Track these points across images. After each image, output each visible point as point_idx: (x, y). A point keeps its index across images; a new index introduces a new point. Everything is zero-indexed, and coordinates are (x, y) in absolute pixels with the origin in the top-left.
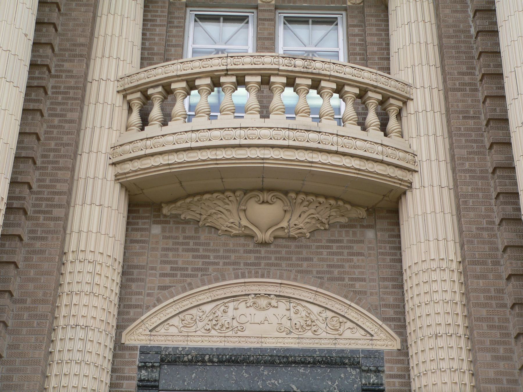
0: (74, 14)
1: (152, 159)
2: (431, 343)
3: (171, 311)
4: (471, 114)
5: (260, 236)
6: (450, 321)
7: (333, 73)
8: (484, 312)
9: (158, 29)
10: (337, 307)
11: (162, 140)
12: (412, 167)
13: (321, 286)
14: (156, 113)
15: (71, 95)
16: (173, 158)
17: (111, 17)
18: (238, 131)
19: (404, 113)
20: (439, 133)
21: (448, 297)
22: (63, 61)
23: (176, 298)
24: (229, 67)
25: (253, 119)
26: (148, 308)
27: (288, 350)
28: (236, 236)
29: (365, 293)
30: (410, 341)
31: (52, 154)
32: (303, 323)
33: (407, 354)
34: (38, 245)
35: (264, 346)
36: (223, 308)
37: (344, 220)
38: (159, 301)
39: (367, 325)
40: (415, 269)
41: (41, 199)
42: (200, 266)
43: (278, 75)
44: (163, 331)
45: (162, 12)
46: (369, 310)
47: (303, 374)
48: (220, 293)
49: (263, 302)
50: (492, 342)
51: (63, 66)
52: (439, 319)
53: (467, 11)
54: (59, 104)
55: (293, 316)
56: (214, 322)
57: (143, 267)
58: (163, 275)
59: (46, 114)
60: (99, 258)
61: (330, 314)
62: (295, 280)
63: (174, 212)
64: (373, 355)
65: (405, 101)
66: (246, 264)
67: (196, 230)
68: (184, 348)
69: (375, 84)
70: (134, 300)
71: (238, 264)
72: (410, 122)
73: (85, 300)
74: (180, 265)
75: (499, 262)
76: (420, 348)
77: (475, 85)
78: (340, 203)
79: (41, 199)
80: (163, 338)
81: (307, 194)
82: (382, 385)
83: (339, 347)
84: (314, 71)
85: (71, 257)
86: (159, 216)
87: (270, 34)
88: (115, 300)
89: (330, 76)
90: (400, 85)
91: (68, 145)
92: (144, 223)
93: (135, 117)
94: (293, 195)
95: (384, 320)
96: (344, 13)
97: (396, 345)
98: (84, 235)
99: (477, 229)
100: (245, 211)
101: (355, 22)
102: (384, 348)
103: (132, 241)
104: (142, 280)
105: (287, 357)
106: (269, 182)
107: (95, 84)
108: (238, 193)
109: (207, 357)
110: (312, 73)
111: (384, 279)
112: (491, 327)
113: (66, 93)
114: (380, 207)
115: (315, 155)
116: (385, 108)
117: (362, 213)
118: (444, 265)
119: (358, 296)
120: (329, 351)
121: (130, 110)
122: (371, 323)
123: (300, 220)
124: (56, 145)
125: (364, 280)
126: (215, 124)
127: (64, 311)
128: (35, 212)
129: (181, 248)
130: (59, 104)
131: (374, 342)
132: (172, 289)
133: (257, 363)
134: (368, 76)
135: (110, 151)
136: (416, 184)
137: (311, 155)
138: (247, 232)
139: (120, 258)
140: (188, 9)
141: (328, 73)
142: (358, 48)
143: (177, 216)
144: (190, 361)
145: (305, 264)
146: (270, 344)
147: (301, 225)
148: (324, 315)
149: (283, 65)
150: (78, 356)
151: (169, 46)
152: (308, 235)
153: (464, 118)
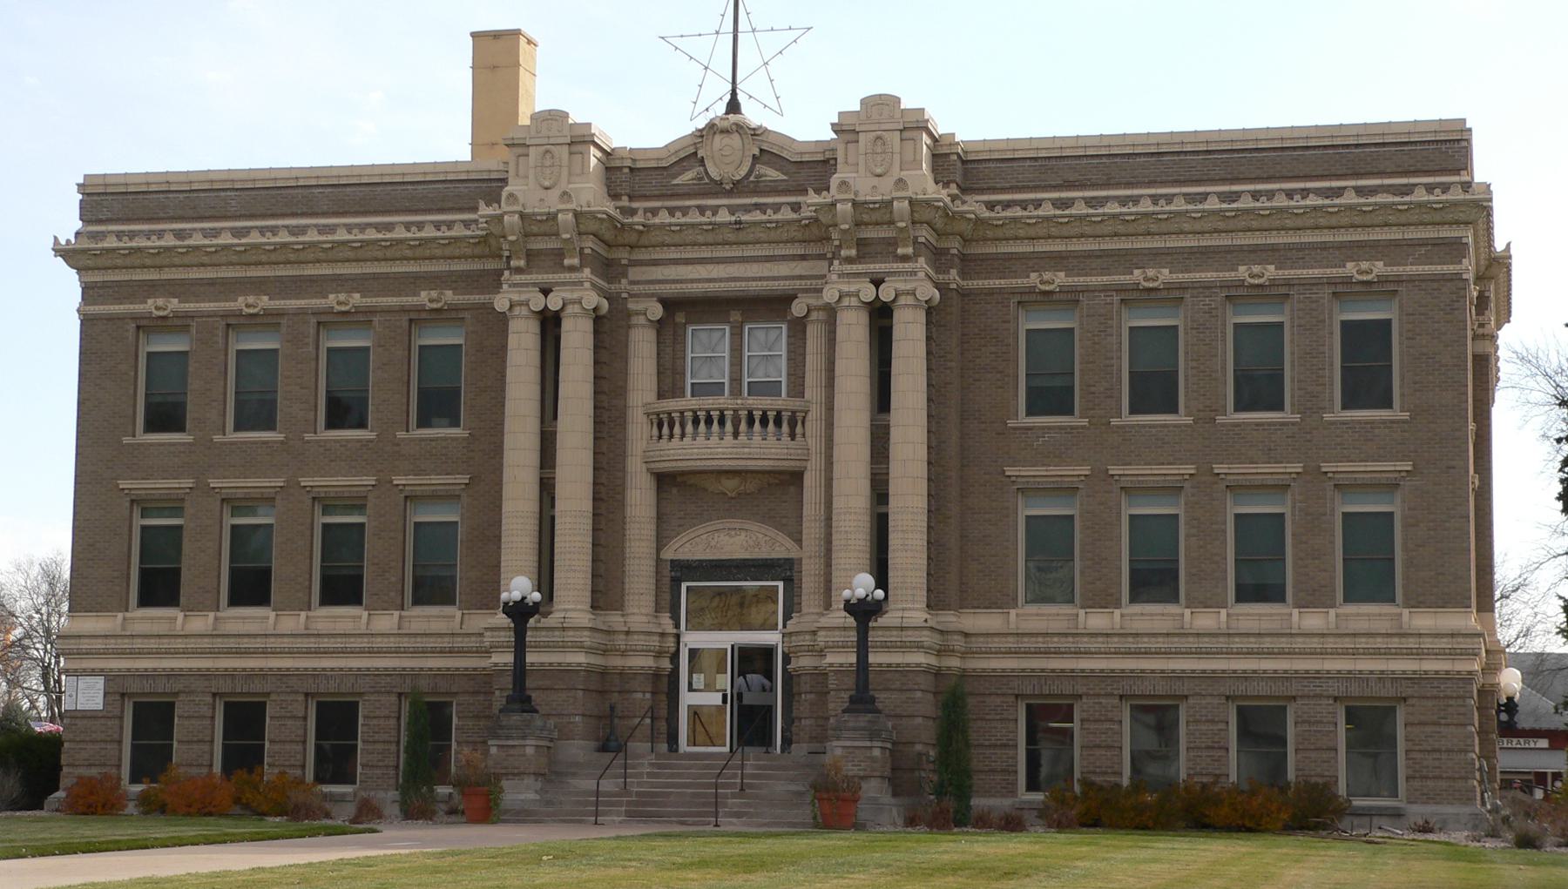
14: (665, 430)
93: (655, 431)
114: (795, 478)
119: (780, 527)
122: (789, 543)
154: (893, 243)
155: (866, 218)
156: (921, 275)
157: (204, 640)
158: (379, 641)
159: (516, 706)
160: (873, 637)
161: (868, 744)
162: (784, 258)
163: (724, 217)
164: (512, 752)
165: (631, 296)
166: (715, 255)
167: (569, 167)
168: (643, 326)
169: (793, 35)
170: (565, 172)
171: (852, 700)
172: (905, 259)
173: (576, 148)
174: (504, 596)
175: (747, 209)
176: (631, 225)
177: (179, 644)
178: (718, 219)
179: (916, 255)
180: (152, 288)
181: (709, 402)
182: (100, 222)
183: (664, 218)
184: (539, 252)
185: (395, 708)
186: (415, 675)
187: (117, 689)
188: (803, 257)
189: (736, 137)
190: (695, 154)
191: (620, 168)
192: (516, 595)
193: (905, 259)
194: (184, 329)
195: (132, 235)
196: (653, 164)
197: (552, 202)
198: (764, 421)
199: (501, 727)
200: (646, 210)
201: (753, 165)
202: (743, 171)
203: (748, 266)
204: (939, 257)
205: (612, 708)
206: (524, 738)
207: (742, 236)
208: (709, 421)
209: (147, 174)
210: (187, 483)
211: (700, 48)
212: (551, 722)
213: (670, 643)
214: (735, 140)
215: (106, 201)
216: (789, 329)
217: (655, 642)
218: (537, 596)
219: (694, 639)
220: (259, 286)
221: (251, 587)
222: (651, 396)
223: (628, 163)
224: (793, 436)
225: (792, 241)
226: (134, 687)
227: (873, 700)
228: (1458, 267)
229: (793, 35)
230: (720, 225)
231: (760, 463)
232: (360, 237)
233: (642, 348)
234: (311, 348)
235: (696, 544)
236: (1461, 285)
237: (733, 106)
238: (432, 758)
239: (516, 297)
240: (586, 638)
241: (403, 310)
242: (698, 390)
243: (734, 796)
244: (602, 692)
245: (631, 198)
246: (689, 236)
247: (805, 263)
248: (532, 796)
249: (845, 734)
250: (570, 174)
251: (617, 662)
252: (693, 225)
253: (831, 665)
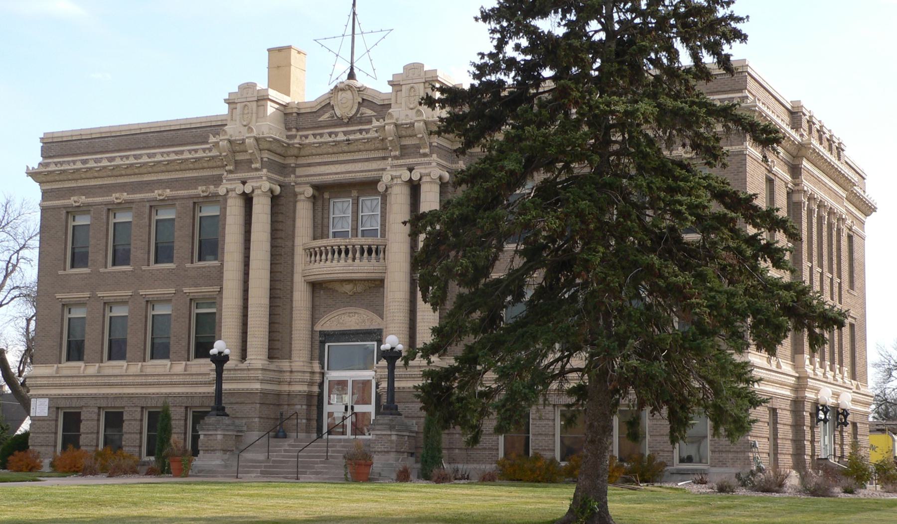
93: (308, 259)
122: (379, 320)
146: (353, 328)
154: (418, 147)
155: (404, 133)
156: (434, 164)
157: (98, 379)
158: (177, 378)
159: (388, 412)
160: (225, 374)
161: (389, 433)
162: (374, 159)
163: (341, 137)
164: (211, 438)
165: (296, 184)
166: (340, 159)
167: (257, 114)
168: (304, 201)
170: (254, 115)
172: (425, 155)
173: (261, 103)
175: (354, 132)
176: (293, 144)
177: (81, 381)
178: (338, 139)
179: (431, 153)
180: (72, 191)
181: (339, 241)
182: (50, 157)
183: (311, 140)
184: (241, 161)
185: (183, 415)
186: (191, 396)
187: (55, 408)
189: (349, 92)
191: (292, 113)
193: (425, 155)
194: (87, 212)
195: (61, 163)
196: (309, 110)
197: (245, 134)
198: (370, 252)
200: (301, 137)
203: (356, 164)
204: (270, 165)
205: (282, 414)
206: (216, 430)
207: (352, 148)
208: (340, 253)
209: (138, 124)
210: (87, 294)
211: (334, 44)
213: (317, 378)
214: (348, 95)
215: (54, 146)
217: (307, 377)
219: (334, 375)
220: (122, 187)
221: (117, 351)
223: (295, 110)
225: (377, 149)
226: (62, 404)
227: (223, 408)
228: (741, 147)
230: (339, 142)
231: (358, 275)
232: (167, 158)
233: (303, 214)
234: (147, 220)
235: (331, 322)
236: (743, 157)
237: (351, 76)
238: (163, 444)
239: (231, 186)
240: (259, 374)
241: (190, 197)
242: (335, 235)
243: (321, 462)
245: (298, 130)
246: (325, 149)
248: (218, 462)
249: (378, 427)
250: (257, 118)
251: (286, 388)
252: (326, 143)
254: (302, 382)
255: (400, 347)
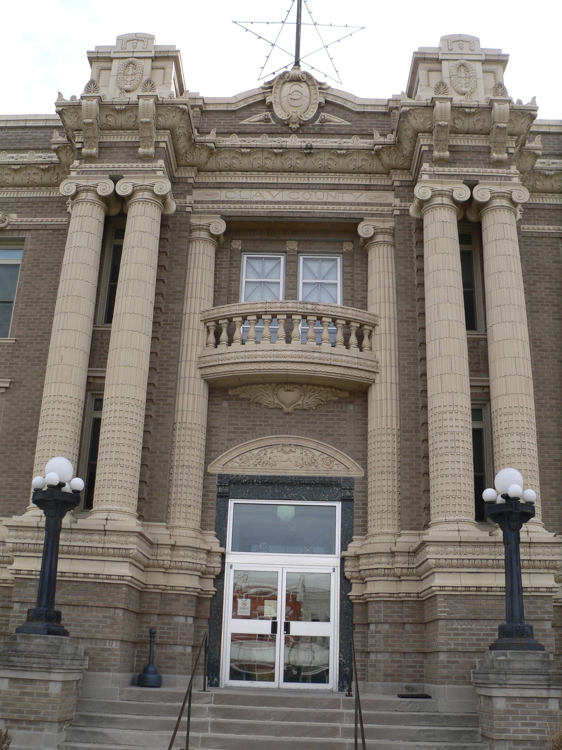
0: (174, 271)
1: (222, 367)
2: (379, 477)
3: (235, 454)
4: (412, 338)
5: (286, 409)
6: (390, 465)
7: (330, 313)
8: (408, 460)
9: (224, 270)
10: (329, 452)
11: (228, 356)
12: (375, 370)
13: (321, 439)
14: (224, 336)
15: (174, 326)
16: (235, 368)
17: (196, 270)
18: (272, 352)
19: (373, 334)
20: (393, 348)
21: (390, 450)
22: (169, 303)
23: (237, 446)
24: (267, 310)
25: (281, 344)
26: (222, 452)
27: (301, 477)
28: (271, 408)
29: (346, 443)
30: (369, 473)
31: (165, 364)
32: (309, 461)
33: (367, 479)
34: (161, 420)
35: (287, 474)
36: (264, 452)
37: (335, 399)
38: (228, 448)
39: (346, 463)
40: (373, 433)
41: (161, 392)
42: (251, 427)
43: (296, 314)
44: (230, 465)
45: (226, 258)
46: (348, 454)
47: (309, 490)
48: (262, 444)
49: (287, 449)
50: (411, 477)
51: (169, 306)
52: (384, 464)
53: (413, 268)
54: (168, 331)
55: (304, 456)
56: (259, 461)
57: (218, 427)
58: (229, 432)
59: (160, 338)
60: (194, 426)
61: (325, 456)
62: (306, 436)
63: (235, 393)
64: (349, 480)
65: (374, 326)
66: (277, 426)
67: (249, 404)
68: (242, 476)
69: (355, 317)
70: (214, 447)
71: (273, 425)
72: (376, 339)
73: (187, 451)
74: (239, 426)
75: (419, 431)
76: (373, 479)
77: (415, 318)
78: (333, 390)
79: (161, 392)
80: (230, 470)
81: (313, 385)
82: (353, 496)
83: (330, 475)
84: (318, 312)
85: (178, 426)
86: (226, 396)
87: (294, 272)
88: (203, 449)
89: (328, 314)
90: (371, 317)
91: (174, 358)
92: (218, 401)
93: (212, 338)
94: (305, 386)
95: (356, 460)
96: (341, 255)
97: (362, 474)
98: (185, 413)
99: (409, 411)
100: (277, 395)
101: (348, 264)
102: (355, 476)
103: (212, 412)
104: (218, 435)
105: (300, 481)
106: (290, 380)
107: (187, 315)
108: (273, 385)
109: (255, 481)
110: (317, 313)
111: (357, 435)
112: (411, 469)
113: (171, 324)
114: (356, 392)
115: (317, 367)
116: (359, 333)
117: (347, 394)
118: (389, 431)
119: (340, 445)
120: (324, 478)
121: (208, 332)
122: (349, 461)
123: (309, 400)
124: (167, 358)
125: (346, 435)
126: (260, 347)
127: (176, 457)
128: (158, 400)
129: (240, 415)
130: (168, 331)
131: (350, 472)
132: (235, 441)
133: (283, 484)
134: (351, 313)
135: (197, 360)
136: (377, 381)
137: (315, 367)
138: (278, 406)
139: (205, 425)
140: (243, 253)
141: (327, 313)
142: (349, 281)
143: (237, 396)
144: (246, 483)
145: (312, 425)
146: (291, 473)
147: (310, 403)
148: (322, 457)
149: (300, 308)
150: (185, 483)
151: (230, 280)
152: (314, 408)
153: (408, 340)
159: (40, 625)
164: (29, 688)
168: (205, 240)
169: (348, 31)
171: (503, 631)
174: (37, 481)
188: (368, 188)
190: (264, 101)
192: (53, 478)
199: (18, 653)
201: (318, 113)
202: (310, 115)
205: (152, 634)
206: (48, 670)
212: (82, 647)
214: (304, 88)
216: (344, 260)
217: (201, 559)
218: (79, 483)
222: (208, 305)
224: (360, 346)
227: (58, 616)
229: (348, 31)
233: (202, 261)
235: (245, 460)
244: (139, 614)
247: (369, 193)
251: (158, 579)
253: (442, 588)
254: (190, 570)
255: (531, 494)
